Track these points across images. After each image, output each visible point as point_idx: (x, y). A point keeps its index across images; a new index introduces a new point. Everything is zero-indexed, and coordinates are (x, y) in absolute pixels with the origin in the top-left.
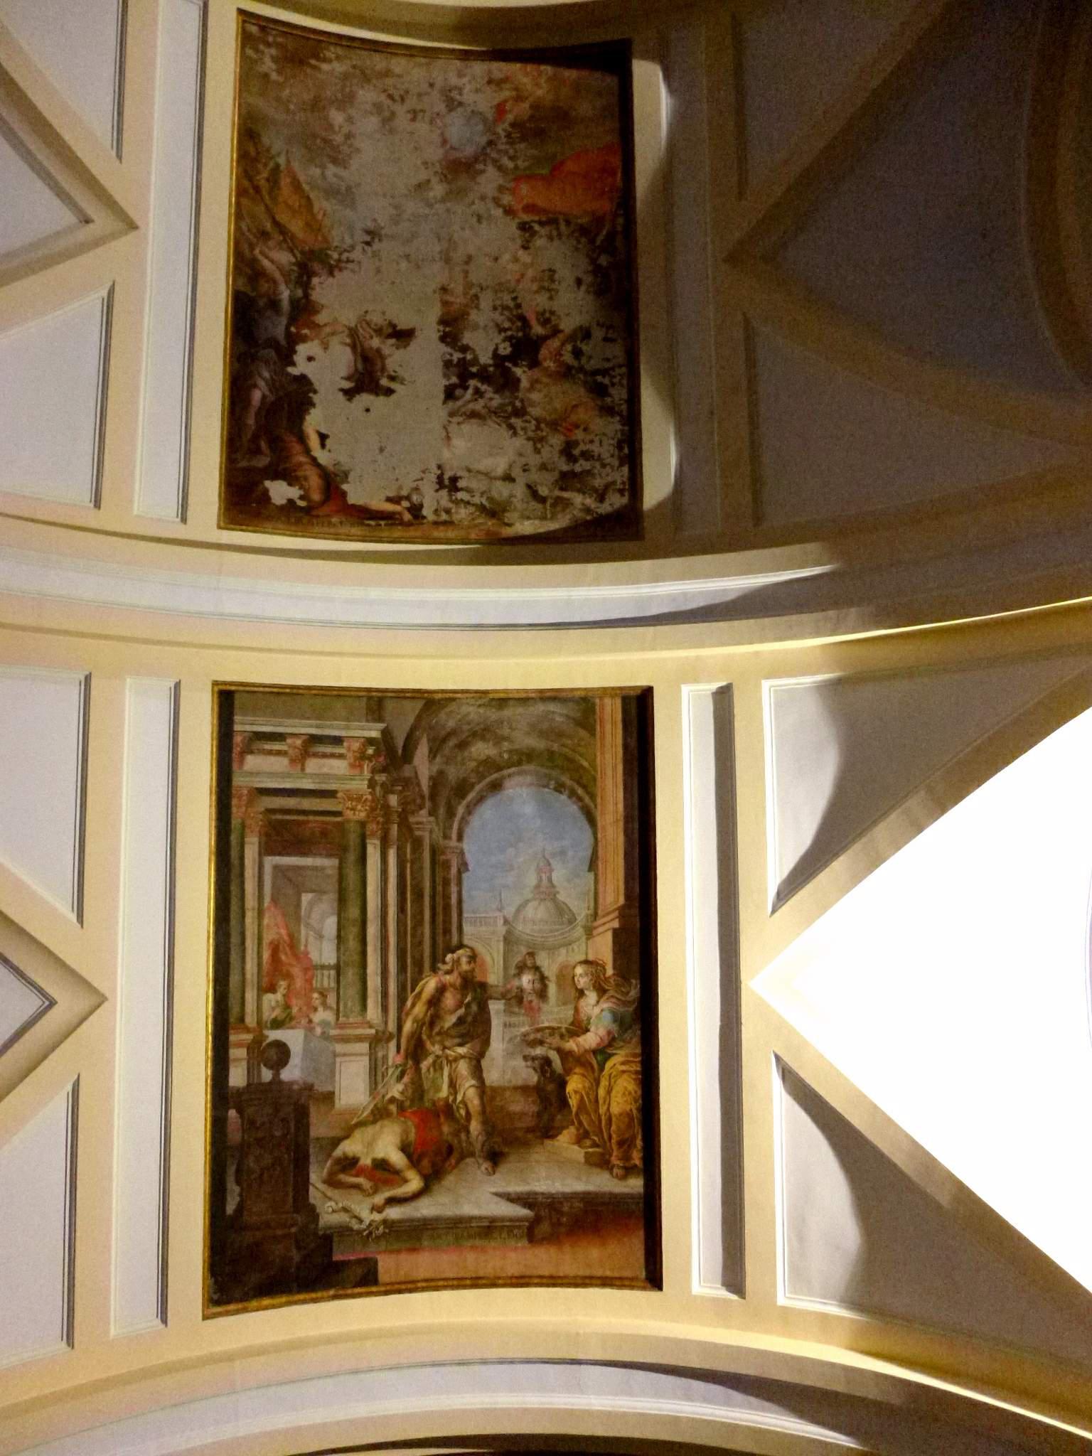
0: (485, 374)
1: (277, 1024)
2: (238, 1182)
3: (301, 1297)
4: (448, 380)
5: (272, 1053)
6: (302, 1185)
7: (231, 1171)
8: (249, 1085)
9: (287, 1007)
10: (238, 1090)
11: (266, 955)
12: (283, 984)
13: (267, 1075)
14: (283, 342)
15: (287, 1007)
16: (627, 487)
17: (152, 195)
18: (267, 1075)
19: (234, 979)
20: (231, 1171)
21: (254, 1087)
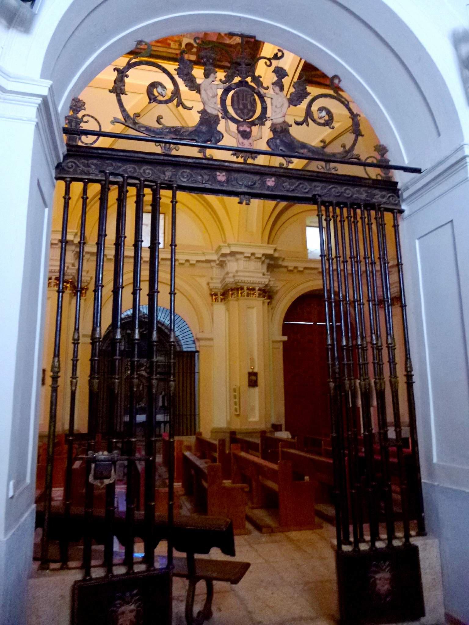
0: (178, 349)
1: (180, 44)
2: (222, 61)
3: (260, 51)
4: (185, 446)
5: (189, 47)
6: (230, 46)
7: (219, 63)
8: (196, 55)
9: (175, 41)
10: (197, 58)
11: (159, 44)
12: (168, 41)
13: (194, 50)
14: (310, 121)
15: (175, 41)
16: (129, 359)
17: (175, 473)
18: (194, 50)
19: (165, 54)
20: (219, 63)
21: (197, 54)
